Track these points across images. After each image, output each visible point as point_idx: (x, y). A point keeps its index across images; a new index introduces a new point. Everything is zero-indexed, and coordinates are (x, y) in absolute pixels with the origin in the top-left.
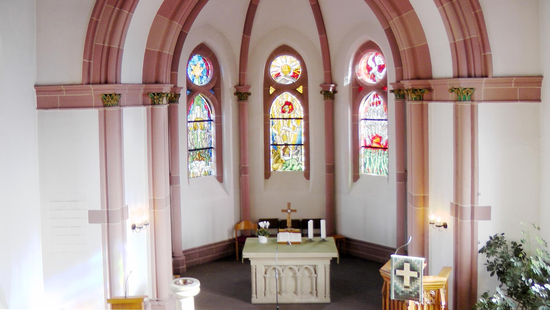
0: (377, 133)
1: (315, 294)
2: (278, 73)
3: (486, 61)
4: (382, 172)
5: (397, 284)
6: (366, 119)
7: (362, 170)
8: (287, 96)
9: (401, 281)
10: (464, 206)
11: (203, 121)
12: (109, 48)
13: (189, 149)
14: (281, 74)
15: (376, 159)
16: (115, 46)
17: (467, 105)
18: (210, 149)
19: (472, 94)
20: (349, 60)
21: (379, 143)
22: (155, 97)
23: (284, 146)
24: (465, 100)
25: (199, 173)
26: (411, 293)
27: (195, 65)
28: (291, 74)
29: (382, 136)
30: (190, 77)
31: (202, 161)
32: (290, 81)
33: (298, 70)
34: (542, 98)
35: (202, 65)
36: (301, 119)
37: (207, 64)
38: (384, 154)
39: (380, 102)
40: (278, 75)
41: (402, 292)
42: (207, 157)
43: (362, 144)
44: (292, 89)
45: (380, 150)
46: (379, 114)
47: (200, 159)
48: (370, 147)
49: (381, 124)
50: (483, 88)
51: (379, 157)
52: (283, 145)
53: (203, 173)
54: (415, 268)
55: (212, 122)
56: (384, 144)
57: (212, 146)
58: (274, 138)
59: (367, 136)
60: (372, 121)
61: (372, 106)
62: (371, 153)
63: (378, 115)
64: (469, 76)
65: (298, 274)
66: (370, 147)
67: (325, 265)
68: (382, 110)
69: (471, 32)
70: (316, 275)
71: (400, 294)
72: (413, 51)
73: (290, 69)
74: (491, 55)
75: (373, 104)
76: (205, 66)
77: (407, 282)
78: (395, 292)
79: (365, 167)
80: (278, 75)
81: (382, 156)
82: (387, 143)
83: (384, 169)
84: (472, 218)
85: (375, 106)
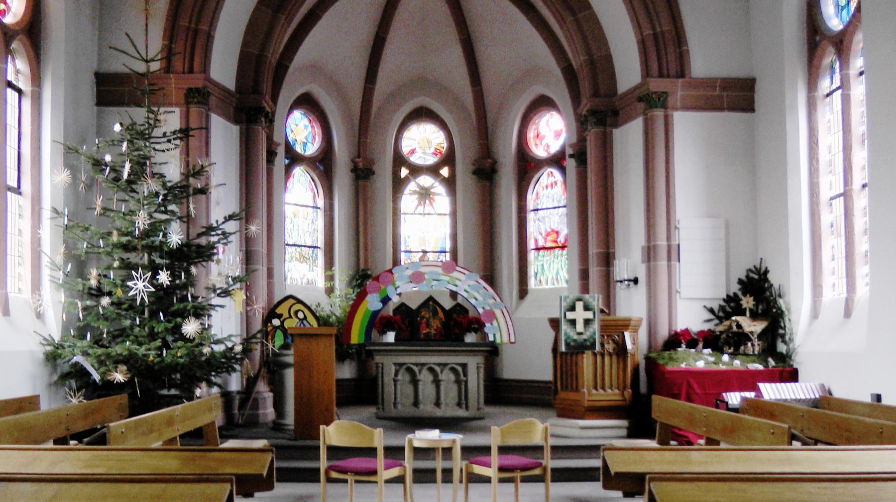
0: (552, 227)
1: (464, 406)
2: (413, 148)
3: (682, 58)
4: (560, 282)
5: (568, 330)
6: (537, 210)
7: (532, 284)
8: (425, 180)
9: (572, 329)
10: (658, 243)
11: (307, 206)
12: (196, 32)
13: (286, 243)
14: (418, 150)
15: (552, 264)
16: (204, 27)
17: (659, 113)
18: (316, 249)
19: (666, 99)
20: (514, 124)
21: (556, 242)
22: (252, 113)
23: (421, 254)
24: (657, 107)
25: (299, 281)
26: (585, 340)
27: (297, 125)
28: (432, 150)
29: (559, 229)
30: (290, 139)
31: (304, 264)
32: (431, 160)
33: (442, 145)
34: (756, 108)
35: (306, 127)
36: (445, 215)
37: (312, 127)
38: (562, 255)
39: (556, 183)
40: (413, 152)
41: (575, 341)
42: (311, 259)
43: (531, 244)
44: (433, 171)
45: (557, 250)
46: (555, 200)
47: (302, 260)
48: (544, 248)
49: (557, 214)
50: (680, 93)
51: (555, 260)
52: (420, 252)
53: (305, 281)
54: (572, 142)
55: (318, 210)
56: (563, 241)
57: (319, 246)
58: (408, 241)
59: (538, 234)
60: (545, 210)
61: (545, 189)
62: (544, 256)
63: (553, 200)
64: (661, 75)
65: (442, 377)
66: (544, 248)
67: (478, 364)
68: (559, 193)
69: (663, 22)
70: (465, 379)
71: (572, 344)
72: (592, 63)
73: (429, 142)
74: (688, 51)
75: (547, 187)
76: (310, 129)
77: (580, 327)
78: (566, 341)
79: (536, 278)
80: (413, 152)
81: (559, 258)
82: (566, 240)
83: (562, 277)
84: (669, 259)
85: (549, 188)
